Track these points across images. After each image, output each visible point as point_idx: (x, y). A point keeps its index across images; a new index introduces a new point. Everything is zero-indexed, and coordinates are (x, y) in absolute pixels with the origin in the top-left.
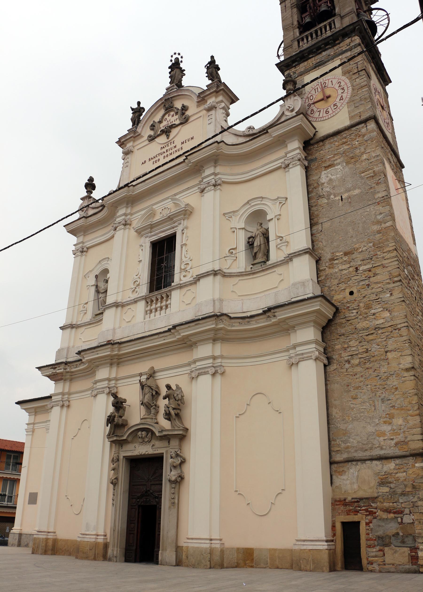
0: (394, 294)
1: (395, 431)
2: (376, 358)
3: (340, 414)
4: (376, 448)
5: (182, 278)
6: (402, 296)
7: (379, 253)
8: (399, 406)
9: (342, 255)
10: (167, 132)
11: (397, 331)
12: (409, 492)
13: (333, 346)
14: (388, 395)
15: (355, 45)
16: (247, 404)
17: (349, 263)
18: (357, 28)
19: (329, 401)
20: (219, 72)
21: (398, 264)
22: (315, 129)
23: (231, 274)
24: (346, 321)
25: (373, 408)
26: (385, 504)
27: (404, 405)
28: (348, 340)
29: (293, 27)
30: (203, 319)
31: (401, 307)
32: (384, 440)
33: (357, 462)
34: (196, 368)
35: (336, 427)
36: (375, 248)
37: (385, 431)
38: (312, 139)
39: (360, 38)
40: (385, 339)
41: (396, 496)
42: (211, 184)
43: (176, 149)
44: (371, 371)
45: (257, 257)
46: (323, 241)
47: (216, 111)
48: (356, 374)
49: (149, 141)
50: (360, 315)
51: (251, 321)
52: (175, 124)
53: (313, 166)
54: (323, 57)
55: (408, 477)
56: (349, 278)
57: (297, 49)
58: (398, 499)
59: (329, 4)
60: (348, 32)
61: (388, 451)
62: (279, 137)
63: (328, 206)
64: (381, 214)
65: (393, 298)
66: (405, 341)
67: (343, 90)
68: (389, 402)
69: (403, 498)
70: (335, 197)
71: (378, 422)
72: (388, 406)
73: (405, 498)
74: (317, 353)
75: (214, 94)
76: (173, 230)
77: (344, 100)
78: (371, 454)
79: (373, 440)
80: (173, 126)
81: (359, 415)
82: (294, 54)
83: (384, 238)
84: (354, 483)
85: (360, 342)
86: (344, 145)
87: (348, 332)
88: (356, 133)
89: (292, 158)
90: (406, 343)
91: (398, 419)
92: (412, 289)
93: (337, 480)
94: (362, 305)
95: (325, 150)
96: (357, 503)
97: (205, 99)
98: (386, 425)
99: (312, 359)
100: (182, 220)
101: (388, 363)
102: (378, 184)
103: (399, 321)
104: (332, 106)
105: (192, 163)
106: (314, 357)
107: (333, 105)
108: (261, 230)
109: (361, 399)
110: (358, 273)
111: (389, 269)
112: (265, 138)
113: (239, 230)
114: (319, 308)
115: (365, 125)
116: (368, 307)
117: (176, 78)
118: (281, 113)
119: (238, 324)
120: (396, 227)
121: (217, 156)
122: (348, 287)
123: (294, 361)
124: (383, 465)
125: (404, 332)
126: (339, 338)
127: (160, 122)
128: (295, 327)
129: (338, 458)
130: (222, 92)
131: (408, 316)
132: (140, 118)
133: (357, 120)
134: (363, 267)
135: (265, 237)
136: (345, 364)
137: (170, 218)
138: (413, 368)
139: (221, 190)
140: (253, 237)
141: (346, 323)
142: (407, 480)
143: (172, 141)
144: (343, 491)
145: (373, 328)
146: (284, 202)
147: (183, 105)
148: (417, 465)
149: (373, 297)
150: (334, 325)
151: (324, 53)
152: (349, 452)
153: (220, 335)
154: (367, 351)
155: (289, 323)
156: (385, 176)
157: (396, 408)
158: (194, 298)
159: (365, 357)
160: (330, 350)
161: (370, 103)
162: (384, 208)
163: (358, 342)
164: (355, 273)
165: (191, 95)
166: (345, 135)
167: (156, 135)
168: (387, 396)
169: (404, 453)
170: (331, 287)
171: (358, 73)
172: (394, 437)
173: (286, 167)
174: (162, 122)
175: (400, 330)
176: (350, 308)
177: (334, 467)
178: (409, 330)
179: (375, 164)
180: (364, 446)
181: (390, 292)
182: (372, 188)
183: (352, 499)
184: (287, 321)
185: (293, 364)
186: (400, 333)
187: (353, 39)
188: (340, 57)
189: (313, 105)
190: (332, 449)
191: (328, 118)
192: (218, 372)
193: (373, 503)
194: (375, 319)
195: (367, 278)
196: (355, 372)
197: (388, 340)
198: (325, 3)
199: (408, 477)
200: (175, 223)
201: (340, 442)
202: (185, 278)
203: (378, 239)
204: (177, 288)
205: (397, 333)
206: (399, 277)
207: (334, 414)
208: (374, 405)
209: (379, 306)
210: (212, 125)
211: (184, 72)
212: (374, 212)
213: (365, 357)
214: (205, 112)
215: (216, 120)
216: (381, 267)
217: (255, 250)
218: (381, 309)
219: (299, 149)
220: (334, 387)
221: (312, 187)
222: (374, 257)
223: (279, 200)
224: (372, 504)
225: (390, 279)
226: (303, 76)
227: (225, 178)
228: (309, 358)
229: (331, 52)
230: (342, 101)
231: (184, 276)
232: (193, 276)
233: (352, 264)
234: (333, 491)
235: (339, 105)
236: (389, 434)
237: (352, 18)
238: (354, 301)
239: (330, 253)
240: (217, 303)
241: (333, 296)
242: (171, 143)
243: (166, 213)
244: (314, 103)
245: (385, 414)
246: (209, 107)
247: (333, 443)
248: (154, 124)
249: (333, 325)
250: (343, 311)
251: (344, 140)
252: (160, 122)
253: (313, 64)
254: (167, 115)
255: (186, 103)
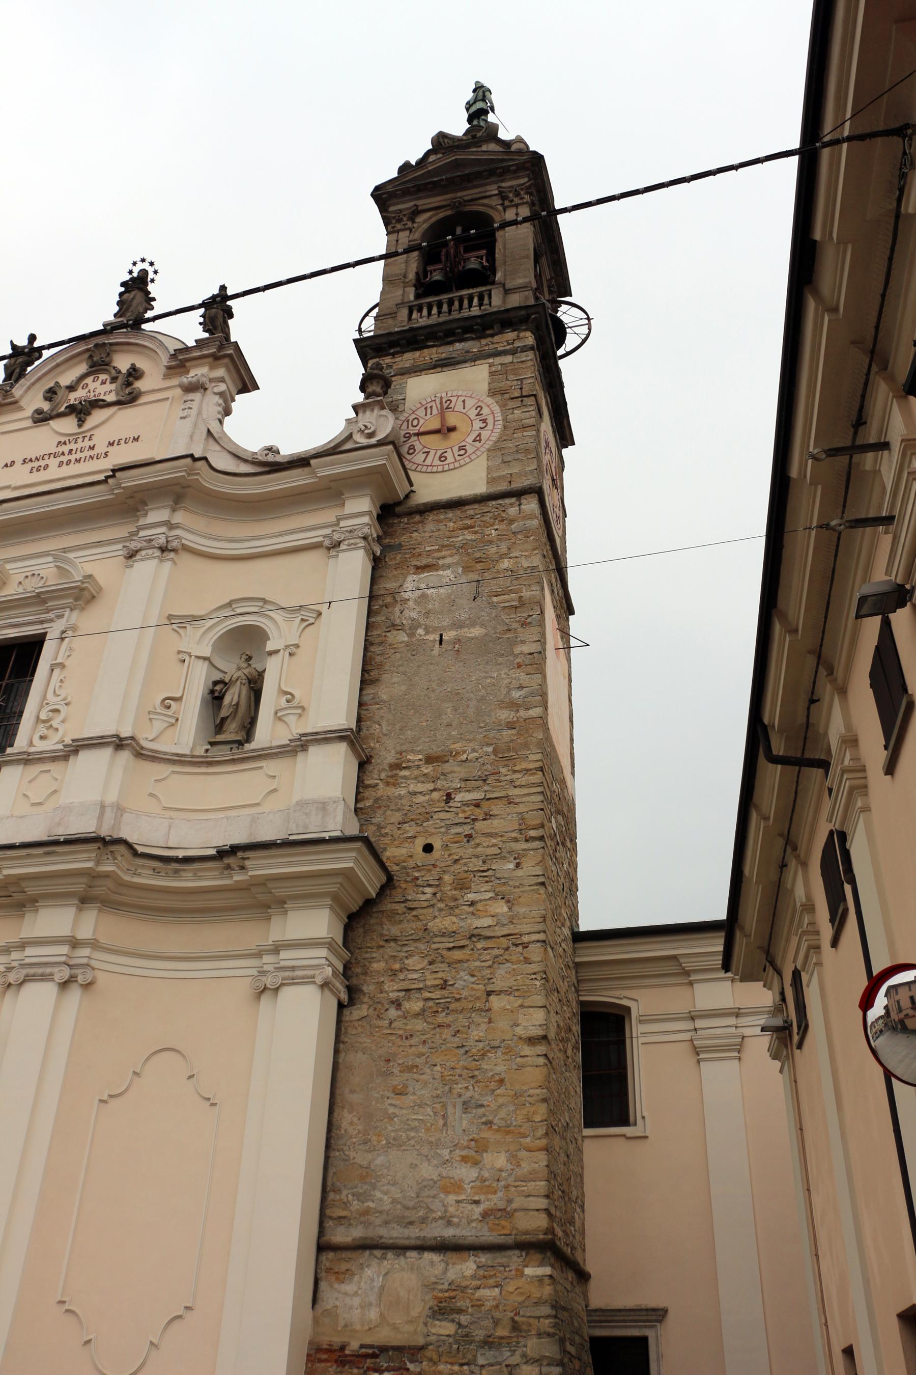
0: (523, 865)
1: (487, 1183)
2: (463, 1004)
3: (360, 1127)
4: (435, 1220)
5: (36, 740)
6: (541, 873)
7: (503, 770)
8: (503, 1124)
9: (420, 760)
10: (81, 411)
11: (520, 949)
12: (502, 1338)
13: (367, 964)
14: (480, 1094)
15: (525, 346)
16: (135, 1073)
17: (433, 782)
18: (533, 316)
19: (338, 1091)
20: (230, 322)
21: (542, 802)
22: (411, 484)
23: (156, 755)
24: (405, 910)
25: (441, 1122)
26: (441, 1367)
27: (515, 1123)
28: (404, 954)
29: (404, 282)
30: (69, 842)
31: (536, 896)
32: (458, 1202)
33: (384, 1251)
34: (23, 962)
35: (344, 1157)
36: (497, 759)
37: (461, 1180)
38: (399, 503)
39: (536, 339)
40: (490, 963)
41: (471, 1347)
42: (154, 543)
43: (91, 453)
44: (447, 1033)
45: (224, 729)
46: (384, 724)
47: (203, 395)
48: (411, 1036)
49: (35, 422)
50: (441, 900)
51: (184, 870)
52: (103, 400)
53: (391, 559)
54: (456, 352)
55: (504, 1299)
56: (428, 813)
57: (405, 324)
58: (475, 1356)
59: (484, 261)
60: (513, 320)
61: (464, 1231)
62: (330, 481)
63: (408, 651)
64: (521, 687)
65: (519, 873)
66: (535, 974)
67: (485, 424)
68: (481, 1110)
69: (487, 1354)
70: (427, 633)
71: (447, 1157)
72: (475, 1121)
73: (492, 1353)
74: (329, 971)
75: (210, 360)
76: (40, 627)
77: (482, 442)
78: (422, 1234)
79: (431, 1199)
80: (97, 404)
81: (404, 1135)
82: (396, 329)
83: (519, 741)
84: (370, 1304)
85: (430, 963)
86: (466, 532)
87: (406, 936)
88: (496, 513)
89: (351, 531)
90: (536, 979)
91: (496, 1154)
92: (559, 864)
93: (331, 1296)
94: (447, 878)
95: (425, 532)
96: (373, 1360)
97: (184, 366)
98: (466, 1165)
99: (314, 983)
100: (68, 610)
101: (490, 1019)
102: (524, 624)
103: (527, 927)
104: (456, 449)
105: (123, 488)
106: (319, 980)
107: (457, 447)
108: (246, 671)
109: (415, 1097)
110: (450, 807)
111: (522, 808)
112: (300, 476)
113: (196, 659)
114: (351, 865)
115: (517, 500)
116: (462, 885)
117: (131, 309)
118: (346, 435)
119: (151, 872)
120: (547, 723)
121: (183, 487)
122: (423, 834)
123: (269, 981)
124: (448, 1265)
125: (535, 952)
126: (383, 947)
127: (71, 388)
128: (285, 903)
129: (340, 1235)
130: (226, 360)
131: (547, 919)
132: (25, 370)
133: (503, 487)
134: (462, 794)
135: (251, 688)
136: (387, 1009)
137: (40, 599)
138: (545, 1037)
139: (174, 563)
140: (226, 684)
141: (404, 913)
142: (501, 1308)
143: (88, 434)
144: (341, 1323)
145: (465, 934)
146: (312, 620)
147: (133, 365)
148: (528, 1271)
149: (477, 864)
150: (376, 915)
151: (458, 346)
152: (367, 1224)
153: (99, 891)
154: (444, 985)
155: (273, 891)
156: (542, 612)
157: (495, 1127)
158: (55, 791)
159: (437, 999)
160: (359, 970)
161: (535, 461)
162: (529, 676)
163: (426, 962)
164: (443, 804)
165: (157, 350)
166: (471, 512)
167: (54, 413)
168: (477, 1096)
169: (501, 1240)
170: (383, 828)
171: (520, 399)
172: (482, 1198)
173: (333, 547)
174: (76, 390)
175: (527, 947)
176: (419, 882)
177: (327, 1259)
178: (546, 949)
179: (526, 583)
180: (407, 1213)
181: (515, 859)
182: (510, 630)
183: (362, 1346)
184: (270, 885)
185: (265, 988)
186: (526, 955)
187: (522, 334)
188: (491, 360)
189: (416, 438)
190: (328, 1212)
191: (443, 471)
192: (77, 981)
193: (411, 1362)
194: (473, 914)
195: (468, 820)
196: (411, 1030)
197: (496, 966)
198: (478, 257)
199: (504, 1299)
200: (48, 613)
201: (350, 1197)
202: (44, 742)
203: (507, 739)
204: (17, 762)
205: (519, 952)
206: (541, 830)
207: (345, 1124)
208: (444, 1116)
209: (487, 887)
210: (188, 423)
211: (152, 303)
212: (506, 682)
213: (437, 999)
214: (179, 391)
215: (199, 413)
216: (504, 801)
217: (224, 713)
218: (491, 895)
219: (370, 516)
220: (355, 1059)
221: (381, 603)
222: (492, 777)
223: (302, 613)
224: (410, 1366)
225: (521, 830)
226: (406, 376)
227: (190, 539)
228: (308, 980)
229: (473, 346)
230: (477, 444)
231: (42, 738)
232: (63, 741)
233: (439, 784)
234: (316, 1321)
235: (470, 449)
236: (471, 1188)
237: (527, 298)
238: (431, 867)
239: (393, 752)
240: (109, 814)
241: (385, 849)
242: (84, 437)
243: (32, 586)
244: (418, 434)
245: (466, 1138)
246: (190, 383)
247: (331, 1196)
248: (57, 389)
249: (373, 913)
250: (404, 886)
251: (469, 522)
252: (71, 388)
253: (431, 359)
254: (92, 378)
255: (142, 364)
